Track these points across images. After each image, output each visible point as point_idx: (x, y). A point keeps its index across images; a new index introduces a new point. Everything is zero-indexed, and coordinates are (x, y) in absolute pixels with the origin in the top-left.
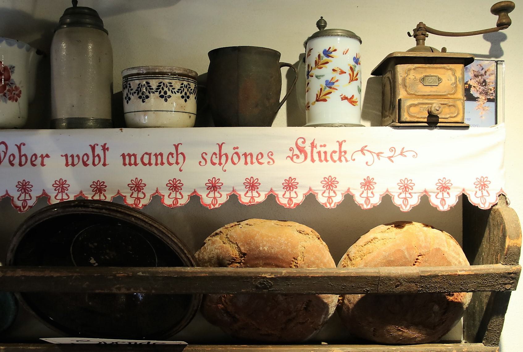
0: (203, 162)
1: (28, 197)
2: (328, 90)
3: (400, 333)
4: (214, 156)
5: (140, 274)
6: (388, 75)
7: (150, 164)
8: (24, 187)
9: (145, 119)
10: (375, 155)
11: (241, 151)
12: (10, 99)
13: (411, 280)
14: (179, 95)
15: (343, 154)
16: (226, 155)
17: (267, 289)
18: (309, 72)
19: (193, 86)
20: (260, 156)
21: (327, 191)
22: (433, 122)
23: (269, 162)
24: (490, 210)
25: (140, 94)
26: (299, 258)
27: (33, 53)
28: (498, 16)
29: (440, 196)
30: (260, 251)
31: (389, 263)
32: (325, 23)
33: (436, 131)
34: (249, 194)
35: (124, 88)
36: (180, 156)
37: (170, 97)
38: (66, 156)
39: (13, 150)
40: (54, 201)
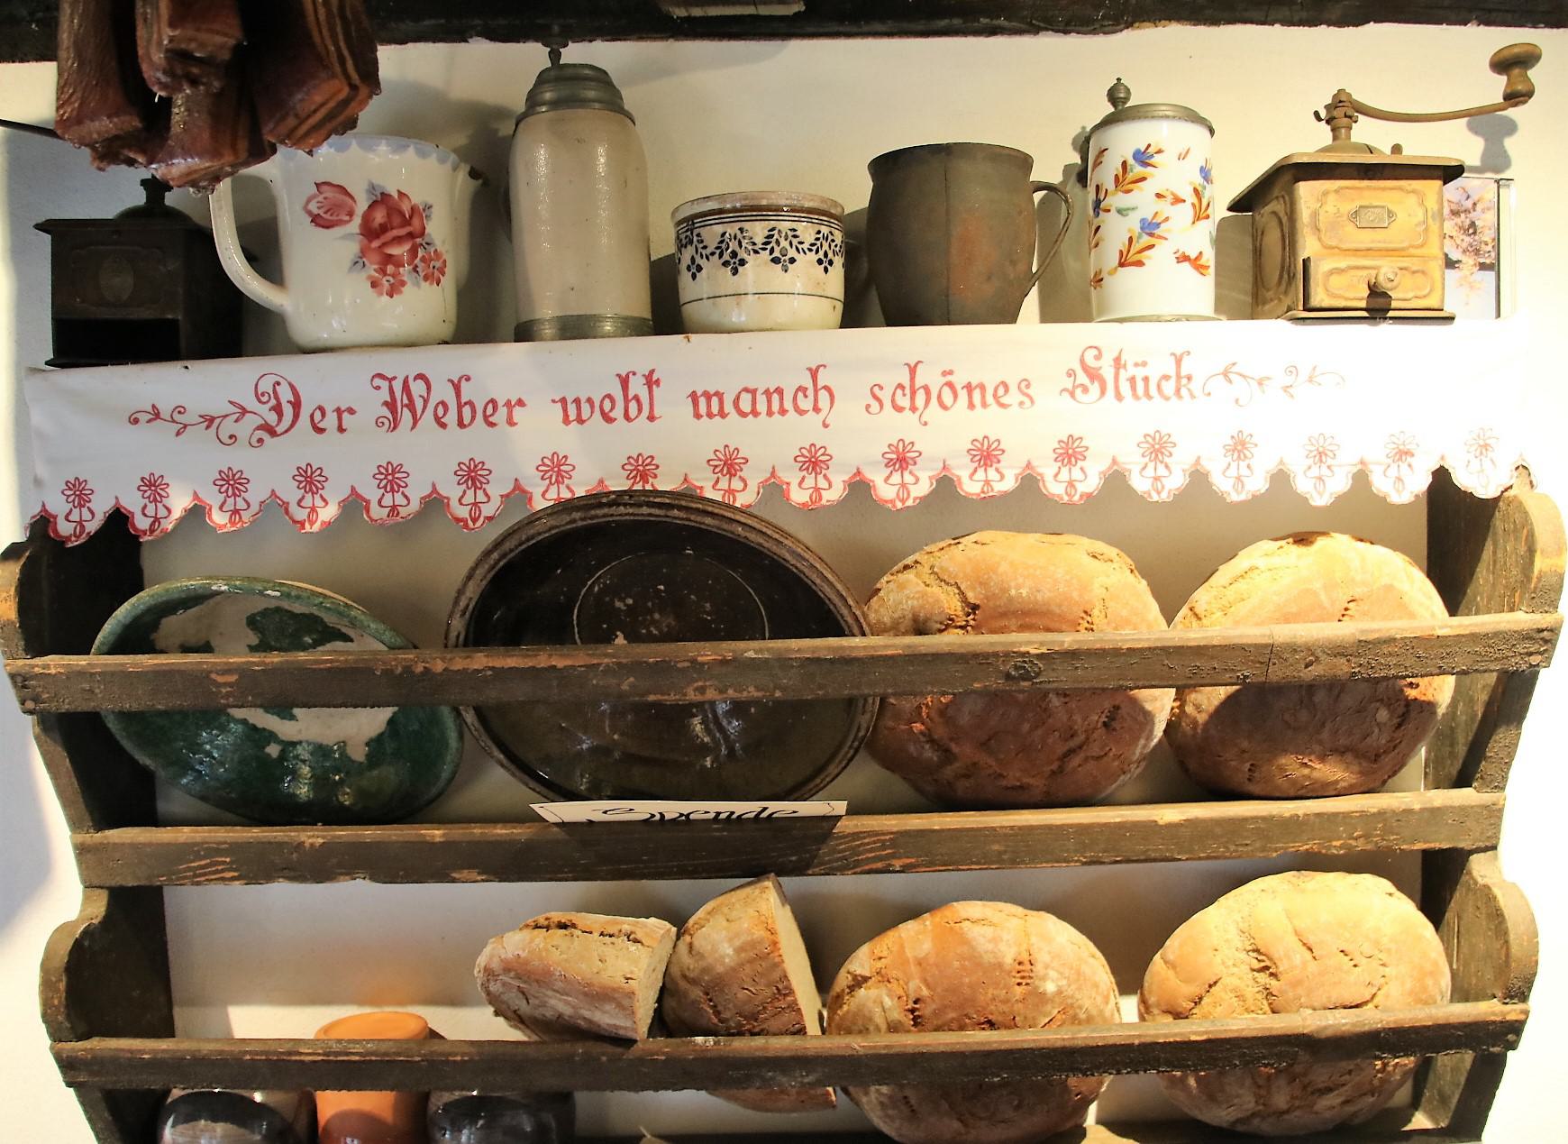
0: (875, 406)
1: (481, 497)
2: (1146, 240)
3: (1306, 771)
4: (899, 392)
5: (751, 654)
6: (1276, 206)
7: (755, 413)
8: (472, 475)
9: (737, 317)
10: (1254, 384)
11: (959, 380)
12: (426, 278)
13: (1339, 650)
14: (813, 257)
15: (1184, 381)
16: (927, 389)
17: (1029, 679)
18: (1098, 203)
19: (838, 236)
20: (1001, 391)
21: (1151, 465)
22: (1378, 307)
23: (1021, 403)
24: (1496, 500)
25: (726, 257)
26: (1096, 612)
27: (462, 174)
28: (1504, 78)
29: (1393, 472)
30: (1011, 599)
31: (1287, 619)
32: (1128, 91)
33: (1385, 329)
34: (980, 475)
35: (681, 246)
36: (823, 395)
37: (792, 261)
38: (563, 401)
39: (442, 391)
40: (540, 504)
